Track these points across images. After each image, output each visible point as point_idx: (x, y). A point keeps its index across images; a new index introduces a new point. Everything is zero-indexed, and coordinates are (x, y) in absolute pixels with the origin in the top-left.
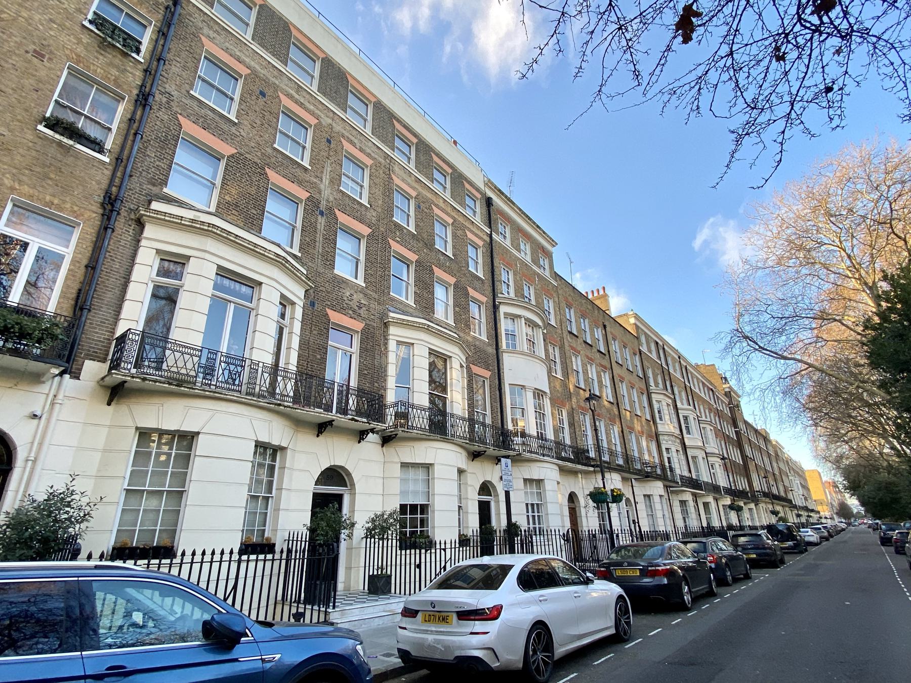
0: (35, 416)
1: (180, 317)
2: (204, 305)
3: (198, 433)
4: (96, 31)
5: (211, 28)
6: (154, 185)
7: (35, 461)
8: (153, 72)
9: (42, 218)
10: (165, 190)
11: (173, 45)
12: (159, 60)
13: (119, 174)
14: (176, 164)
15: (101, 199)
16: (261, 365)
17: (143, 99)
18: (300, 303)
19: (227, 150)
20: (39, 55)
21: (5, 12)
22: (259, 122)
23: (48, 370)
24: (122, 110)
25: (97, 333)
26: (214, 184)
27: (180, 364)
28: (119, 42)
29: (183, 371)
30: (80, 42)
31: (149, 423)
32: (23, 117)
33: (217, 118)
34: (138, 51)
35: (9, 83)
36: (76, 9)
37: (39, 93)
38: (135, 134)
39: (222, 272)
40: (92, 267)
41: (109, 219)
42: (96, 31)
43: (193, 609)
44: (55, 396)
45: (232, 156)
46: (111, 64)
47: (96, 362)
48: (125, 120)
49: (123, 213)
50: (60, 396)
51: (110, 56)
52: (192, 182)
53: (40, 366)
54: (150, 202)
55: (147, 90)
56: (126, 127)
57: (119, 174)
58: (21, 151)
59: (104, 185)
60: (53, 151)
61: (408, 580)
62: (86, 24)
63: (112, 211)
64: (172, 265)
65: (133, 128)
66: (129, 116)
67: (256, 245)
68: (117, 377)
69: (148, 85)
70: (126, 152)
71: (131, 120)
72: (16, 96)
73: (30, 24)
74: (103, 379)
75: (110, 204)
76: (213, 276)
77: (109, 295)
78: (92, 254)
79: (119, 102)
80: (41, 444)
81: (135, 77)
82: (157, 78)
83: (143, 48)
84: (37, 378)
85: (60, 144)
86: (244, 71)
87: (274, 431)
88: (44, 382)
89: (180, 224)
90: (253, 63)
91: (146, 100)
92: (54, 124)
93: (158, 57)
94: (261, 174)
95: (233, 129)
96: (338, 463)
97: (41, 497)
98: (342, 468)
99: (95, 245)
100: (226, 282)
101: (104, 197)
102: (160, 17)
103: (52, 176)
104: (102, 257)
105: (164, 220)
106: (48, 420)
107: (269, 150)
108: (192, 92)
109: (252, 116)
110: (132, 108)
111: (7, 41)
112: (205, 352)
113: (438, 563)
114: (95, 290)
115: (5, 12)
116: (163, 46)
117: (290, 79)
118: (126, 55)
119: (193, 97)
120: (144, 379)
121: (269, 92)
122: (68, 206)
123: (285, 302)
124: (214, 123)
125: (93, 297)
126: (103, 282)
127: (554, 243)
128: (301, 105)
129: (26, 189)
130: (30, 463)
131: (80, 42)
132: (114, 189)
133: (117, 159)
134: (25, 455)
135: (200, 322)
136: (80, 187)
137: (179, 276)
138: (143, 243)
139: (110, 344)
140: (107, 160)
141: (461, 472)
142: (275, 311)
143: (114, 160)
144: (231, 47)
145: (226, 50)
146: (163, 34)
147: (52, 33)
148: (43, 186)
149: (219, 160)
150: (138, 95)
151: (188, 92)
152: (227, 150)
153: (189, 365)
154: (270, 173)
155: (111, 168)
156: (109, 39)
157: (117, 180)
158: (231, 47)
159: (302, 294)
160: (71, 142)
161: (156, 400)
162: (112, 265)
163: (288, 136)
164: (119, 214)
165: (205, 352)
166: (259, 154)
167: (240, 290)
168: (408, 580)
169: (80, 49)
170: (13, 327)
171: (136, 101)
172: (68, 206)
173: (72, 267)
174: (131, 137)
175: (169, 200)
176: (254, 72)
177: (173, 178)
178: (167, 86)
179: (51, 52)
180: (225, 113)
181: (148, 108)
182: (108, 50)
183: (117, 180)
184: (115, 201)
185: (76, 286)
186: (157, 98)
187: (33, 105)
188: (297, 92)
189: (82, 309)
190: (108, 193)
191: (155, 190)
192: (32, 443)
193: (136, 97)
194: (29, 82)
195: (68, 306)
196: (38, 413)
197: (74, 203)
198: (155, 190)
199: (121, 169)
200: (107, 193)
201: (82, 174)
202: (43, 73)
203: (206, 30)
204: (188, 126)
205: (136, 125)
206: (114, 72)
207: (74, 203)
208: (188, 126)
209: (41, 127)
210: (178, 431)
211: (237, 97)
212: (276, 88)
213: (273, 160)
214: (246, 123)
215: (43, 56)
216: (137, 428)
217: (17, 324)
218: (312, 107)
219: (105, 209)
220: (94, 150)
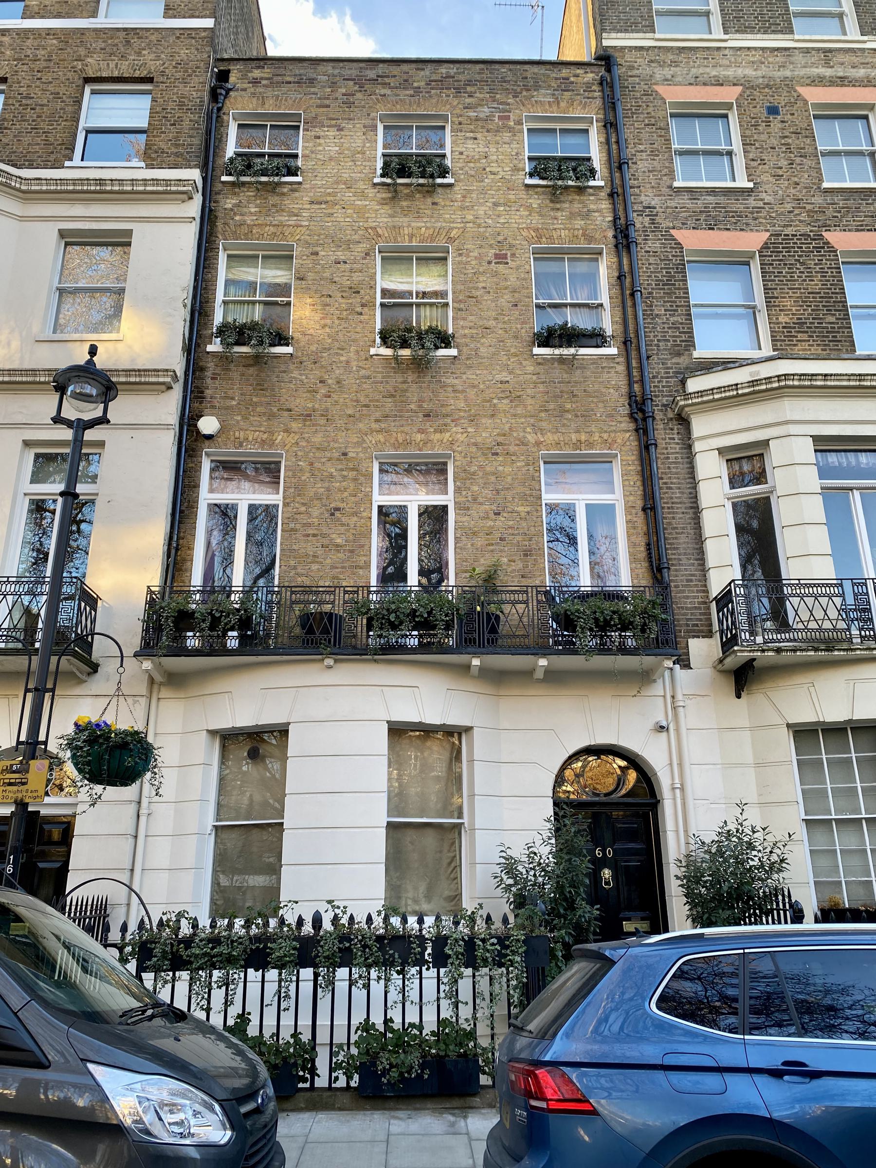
0: (662, 727)
1: (788, 543)
2: (815, 509)
4: (542, 182)
5: (662, 64)
6: (679, 354)
7: (682, 789)
8: (620, 191)
9: (567, 466)
10: (696, 354)
11: (628, 133)
12: (620, 168)
13: (634, 363)
14: (696, 305)
15: (626, 410)
17: (624, 239)
19: (752, 240)
20: (501, 258)
21: (452, 228)
22: (784, 163)
23: (660, 664)
24: (604, 270)
25: (688, 597)
26: (754, 308)
27: (819, 614)
28: (570, 178)
29: (813, 625)
30: (529, 208)
31: (806, 716)
32: (516, 347)
33: (722, 200)
34: (593, 172)
35: (489, 314)
36: (512, 170)
37: (519, 307)
38: (632, 295)
39: (824, 444)
40: (650, 507)
41: (646, 432)
42: (542, 182)
44: (673, 697)
45: (765, 246)
46: (572, 216)
47: (701, 639)
48: (614, 281)
49: (659, 415)
50: (679, 697)
51: (567, 205)
52: (726, 322)
53: (648, 660)
54: (683, 382)
55: (623, 221)
56: (618, 292)
57: (634, 363)
58: (529, 391)
59: (624, 390)
60: (558, 373)
62: (529, 181)
63: (644, 419)
64: (748, 463)
65: (627, 286)
66: (616, 274)
67: (861, 377)
68: (741, 654)
69: (621, 213)
70: (631, 327)
71: (620, 277)
72: (500, 325)
73: (479, 226)
74: (721, 661)
75: (640, 410)
76: (811, 457)
77: (683, 539)
78: (644, 490)
79: (597, 260)
80: (680, 765)
81: (601, 213)
82: (628, 196)
83: (597, 164)
84: (645, 678)
85: (561, 360)
86: (730, 94)
88: (655, 681)
89: (738, 395)
90: (740, 72)
91: (627, 236)
92: (547, 338)
93: (618, 164)
94: (818, 249)
95: (752, 202)
97: (709, 837)
99: (643, 476)
100: (832, 458)
101: (630, 405)
102: (598, 102)
103: (568, 406)
104: (656, 488)
105: (714, 400)
106: (677, 730)
107: (818, 200)
108: (676, 184)
109: (770, 158)
110: (615, 259)
111: (467, 263)
112: (847, 585)
114: (665, 539)
115: (452, 228)
116: (617, 142)
117: (807, 51)
118: (581, 190)
119: (680, 190)
120: (778, 650)
121: (781, 100)
122: (596, 437)
124: (721, 209)
125: (666, 549)
126: (670, 524)
128: (842, 81)
129: (550, 438)
130: (678, 791)
131: (529, 208)
132: (637, 387)
133: (625, 343)
134: (670, 782)
135: (819, 539)
136: (601, 405)
137: (760, 477)
138: (698, 446)
139: (709, 608)
140: (613, 351)
143: (622, 347)
144: (701, 70)
145: (696, 81)
146: (611, 124)
147: (502, 221)
148: (564, 425)
149: (748, 264)
150: (615, 237)
151: (670, 187)
152: (752, 240)
153: (833, 613)
154: (834, 237)
155: (621, 359)
156: (560, 183)
157: (635, 373)
158: (701, 70)
160: (572, 351)
161: (802, 680)
162: (671, 495)
163: (837, 153)
164: (654, 419)
165: (847, 585)
166: (804, 216)
167: (849, 463)
169: (536, 220)
170: (611, 619)
171: (616, 246)
172: (596, 437)
173: (629, 517)
174: (629, 303)
175: (709, 366)
176: (748, 85)
177: (700, 328)
178: (643, 198)
179: (511, 246)
180: (730, 184)
181: (633, 247)
182: (562, 198)
183: (635, 373)
184: (644, 403)
185: (641, 541)
186: (638, 225)
187: (519, 326)
188: (827, 64)
189: (660, 570)
190: (631, 395)
191: (683, 361)
192: (671, 764)
193: (613, 241)
194: (505, 300)
195: (643, 568)
196: (664, 724)
197: (602, 431)
198: (683, 361)
199: (634, 354)
200: (630, 398)
201: (596, 387)
202: (512, 281)
203: (660, 73)
204: (691, 239)
205: (628, 280)
206: (579, 223)
207: (602, 431)
208: (691, 239)
209: (537, 350)
210: (850, 721)
211: (737, 146)
212: (789, 84)
213: (830, 212)
214: (766, 178)
215: (505, 256)
216: (789, 726)
217: (614, 612)
218: (861, 72)
219: (636, 420)
220: (597, 346)
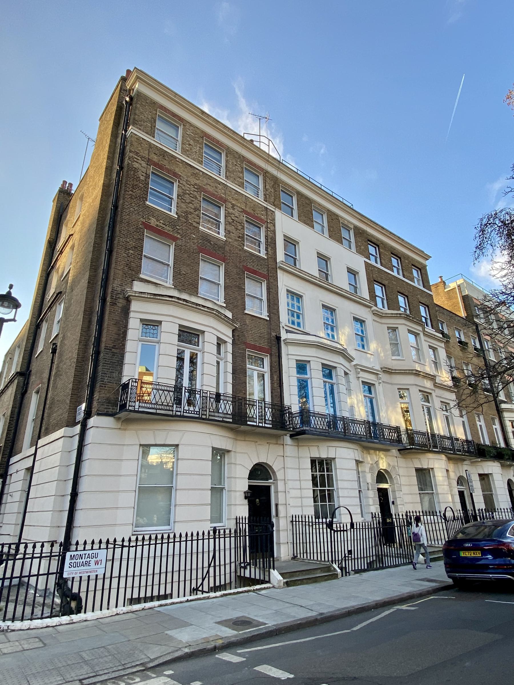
3: (212, 447)
16: (208, 392)
18: (230, 341)
43: (116, 577)
61: (322, 540)
87: (220, 439)
96: (262, 460)
98: (266, 464)
113: (122, 591)
123: (220, 343)
127: (427, 257)
138: (132, 315)
141: (358, 462)
142: (214, 349)
159: (230, 334)
168: (322, 540)
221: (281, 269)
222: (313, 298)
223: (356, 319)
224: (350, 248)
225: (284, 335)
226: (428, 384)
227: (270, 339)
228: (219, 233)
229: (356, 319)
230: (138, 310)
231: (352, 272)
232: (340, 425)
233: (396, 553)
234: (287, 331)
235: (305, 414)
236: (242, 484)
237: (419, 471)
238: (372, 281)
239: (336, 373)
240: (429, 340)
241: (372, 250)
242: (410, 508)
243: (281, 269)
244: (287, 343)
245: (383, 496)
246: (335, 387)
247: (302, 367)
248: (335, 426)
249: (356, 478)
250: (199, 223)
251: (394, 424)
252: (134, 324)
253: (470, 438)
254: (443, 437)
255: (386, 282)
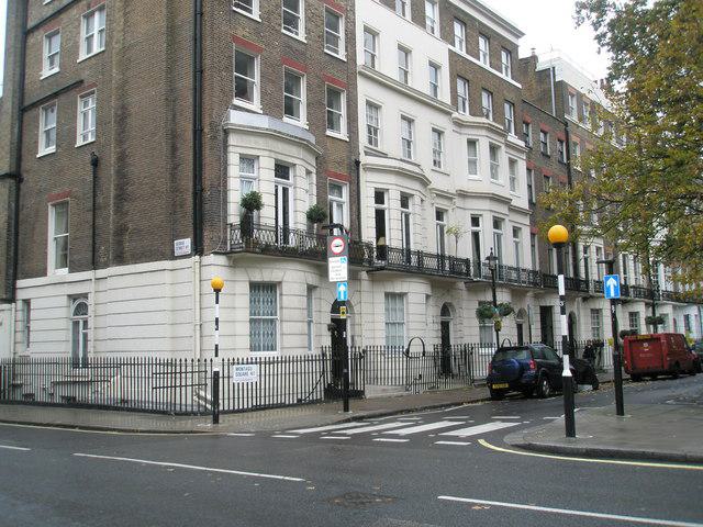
127: (519, 34)
138: (230, 149)
221: (361, 74)
222: (392, 106)
223: (404, 118)
224: (404, 15)
225: (364, 159)
226: (503, 209)
227: (349, 164)
228: (297, 34)
229: (404, 118)
230: (237, 147)
231: (435, 67)
232: (414, 259)
233: (183, 402)
234: (366, 153)
235: (383, 251)
236: (327, 319)
237: (631, 314)
238: (456, 75)
239: (295, 170)
240: (512, 152)
241: (458, 29)
242: (467, 340)
243: (361, 74)
244: (366, 169)
245: (338, 327)
246: (411, 217)
247: (379, 197)
248: (409, 260)
249: (305, 306)
250: (280, 25)
251: (464, 257)
252: (233, 159)
253: (538, 269)
254: (510, 268)
255: (469, 77)
